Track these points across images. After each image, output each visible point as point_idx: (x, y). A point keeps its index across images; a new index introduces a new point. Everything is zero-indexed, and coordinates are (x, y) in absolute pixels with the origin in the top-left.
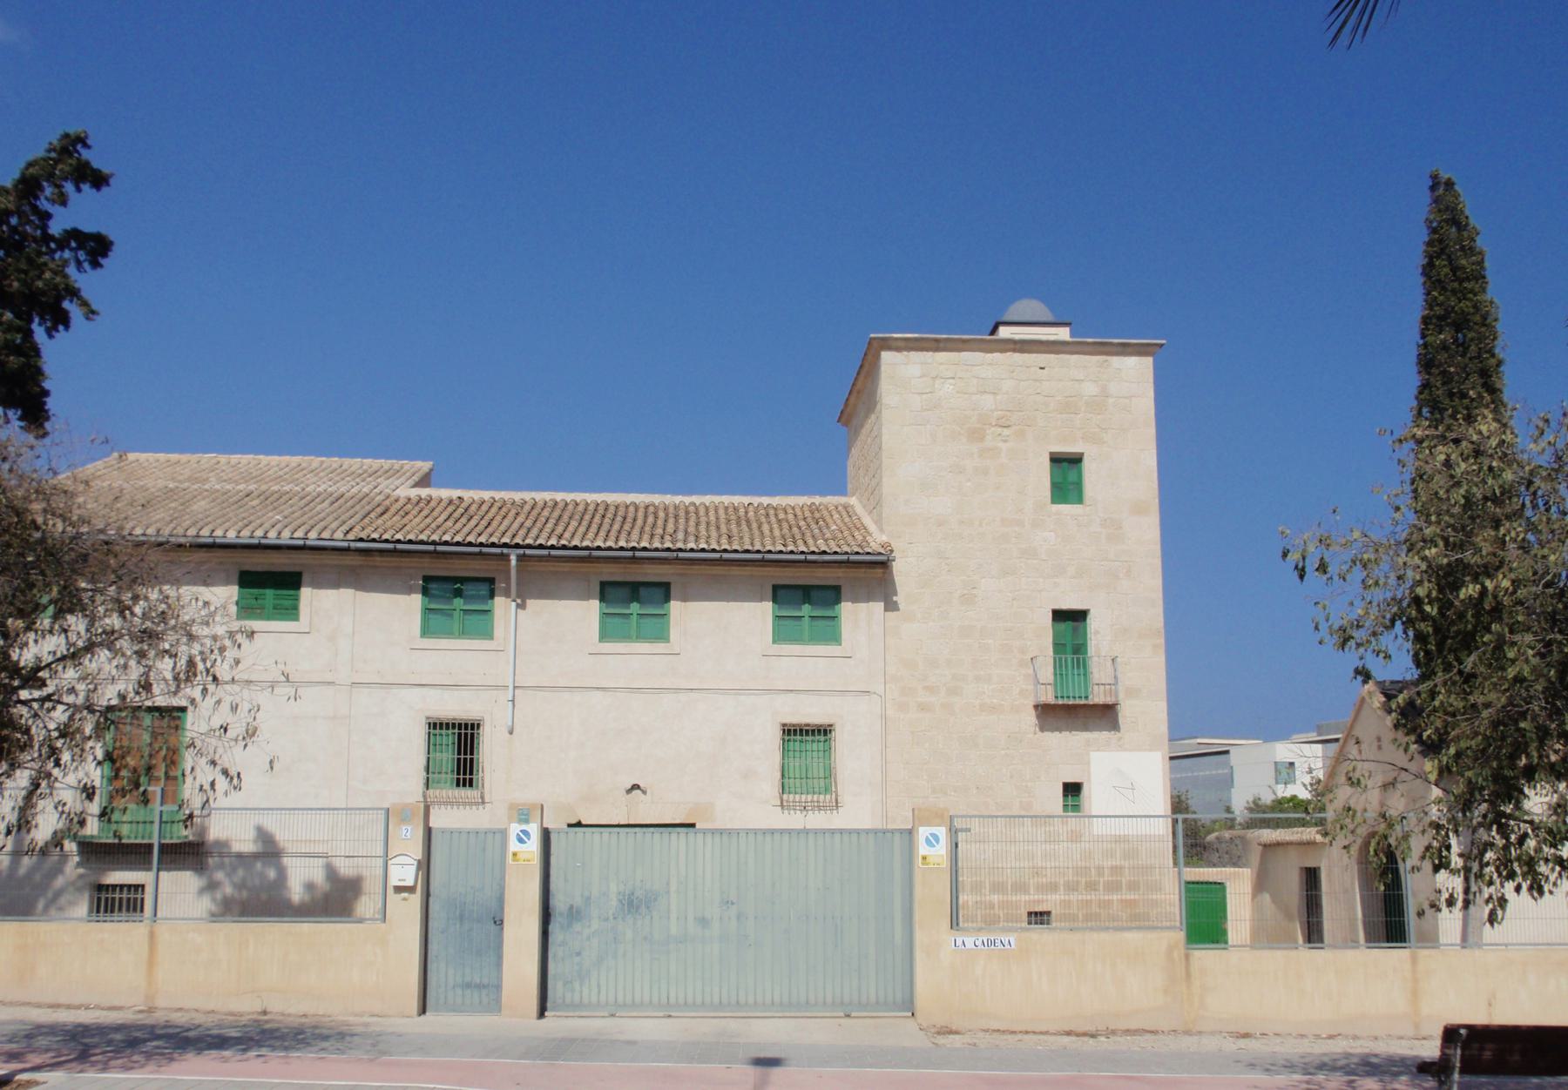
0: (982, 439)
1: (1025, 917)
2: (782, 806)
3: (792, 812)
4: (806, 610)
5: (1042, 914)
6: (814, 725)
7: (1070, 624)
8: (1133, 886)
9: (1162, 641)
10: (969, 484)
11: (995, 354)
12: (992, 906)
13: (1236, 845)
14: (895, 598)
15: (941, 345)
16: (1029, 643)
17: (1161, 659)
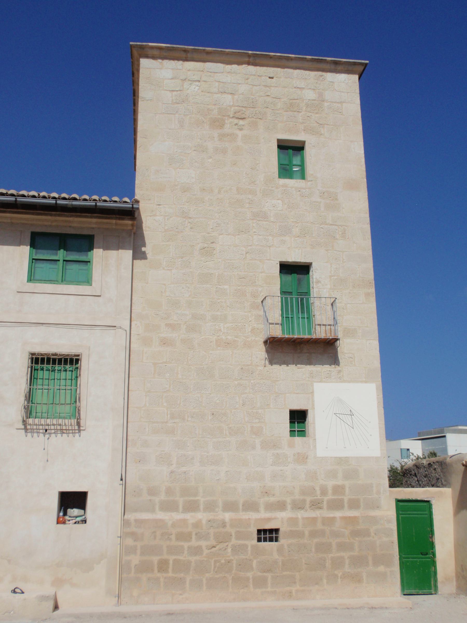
0: (222, 126)
1: (255, 536)
2: (26, 429)
3: (35, 435)
4: (61, 254)
5: (271, 531)
6: (60, 355)
7: (295, 276)
8: (354, 504)
9: (373, 290)
10: (210, 160)
11: (233, 66)
12: (224, 525)
13: (435, 469)
14: (143, 249)
15: (189, 55)
16: (260, 289)
17: (372, 305)
